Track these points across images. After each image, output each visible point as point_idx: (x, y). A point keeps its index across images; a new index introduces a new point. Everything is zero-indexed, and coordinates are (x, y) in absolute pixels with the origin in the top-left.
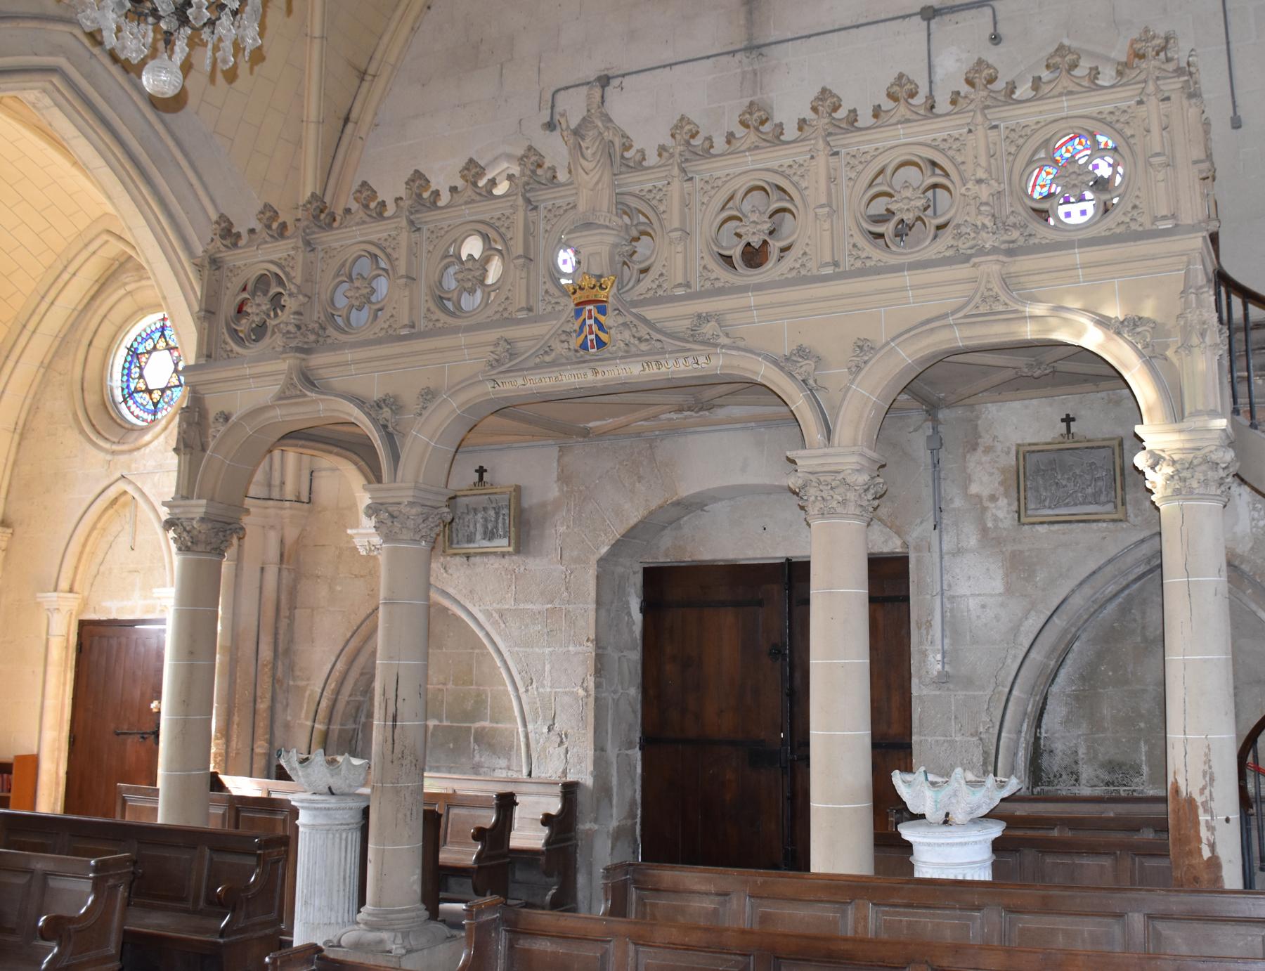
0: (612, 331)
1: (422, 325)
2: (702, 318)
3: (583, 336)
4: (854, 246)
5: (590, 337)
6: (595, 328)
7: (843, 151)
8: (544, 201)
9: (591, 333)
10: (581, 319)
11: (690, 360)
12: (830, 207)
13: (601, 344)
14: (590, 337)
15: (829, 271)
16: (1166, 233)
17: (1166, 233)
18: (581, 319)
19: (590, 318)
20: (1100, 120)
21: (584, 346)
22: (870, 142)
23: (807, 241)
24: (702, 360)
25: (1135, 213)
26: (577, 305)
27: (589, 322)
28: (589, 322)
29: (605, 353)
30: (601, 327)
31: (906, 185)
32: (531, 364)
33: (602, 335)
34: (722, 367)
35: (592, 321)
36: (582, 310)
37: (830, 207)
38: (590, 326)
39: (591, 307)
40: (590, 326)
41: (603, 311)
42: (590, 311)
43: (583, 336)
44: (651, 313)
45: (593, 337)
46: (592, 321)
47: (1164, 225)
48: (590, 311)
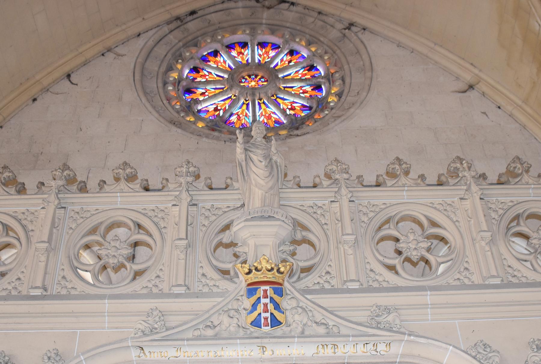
0: (288, 313)
1: (55, 290)
2: (388, 310)
3: (256, 314)
4: (64, 277)
5: (264, 315)
6: (271, 307)
7: (70, 208)
8: (204, 201)
9: (266, 311)
10: (255, 298)
11: (370, 346)
12: (50, 244)
13: (275, 322)
14: (264, 315)
15: (38, 292)
16: (178, 296)
17: (178, 296)
18: (255, 298)
19: (266, 297)
20: (144, 214)
21: (256, 323)
22: (507, 195)
23: (23, 270)
24: (381, 347)
25: (157, 281)
26: (249, 285)
27: (263, 301)
28: (263, 301)
29: (278, 331)
30: (277, 307)
31: (116, 238)
32: (190, 336)
33: (276, 313)
34: (403, 355)
35: (267, 301)
36: (256, 289)
37: (50, 244)
38: (266, 305)
39: (267, 287)
40: (266, 305)
41: (279, 292)
42: (265, 291)
43: (256, 314)
44: (325, 300)
45: (268, 315)
46: (267, 301)
47: (177, 290)
48: (265, 291)
